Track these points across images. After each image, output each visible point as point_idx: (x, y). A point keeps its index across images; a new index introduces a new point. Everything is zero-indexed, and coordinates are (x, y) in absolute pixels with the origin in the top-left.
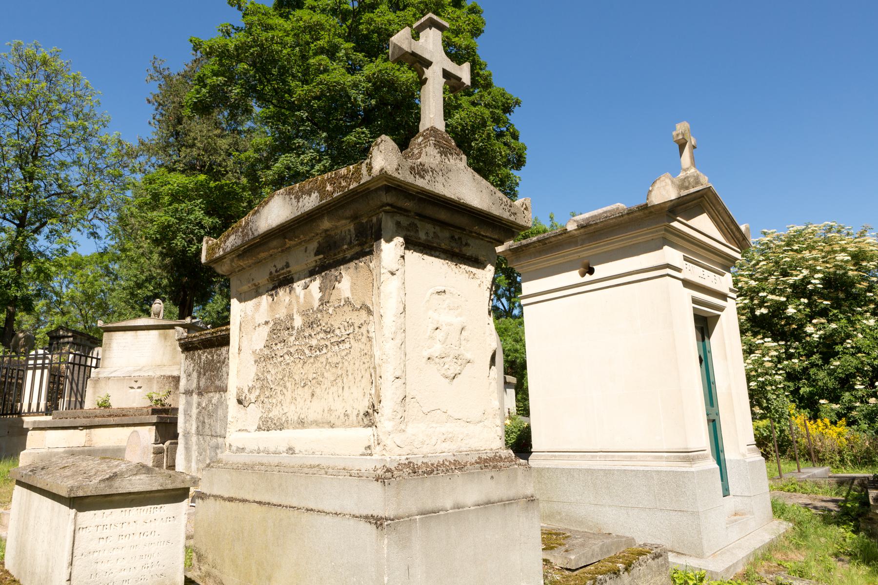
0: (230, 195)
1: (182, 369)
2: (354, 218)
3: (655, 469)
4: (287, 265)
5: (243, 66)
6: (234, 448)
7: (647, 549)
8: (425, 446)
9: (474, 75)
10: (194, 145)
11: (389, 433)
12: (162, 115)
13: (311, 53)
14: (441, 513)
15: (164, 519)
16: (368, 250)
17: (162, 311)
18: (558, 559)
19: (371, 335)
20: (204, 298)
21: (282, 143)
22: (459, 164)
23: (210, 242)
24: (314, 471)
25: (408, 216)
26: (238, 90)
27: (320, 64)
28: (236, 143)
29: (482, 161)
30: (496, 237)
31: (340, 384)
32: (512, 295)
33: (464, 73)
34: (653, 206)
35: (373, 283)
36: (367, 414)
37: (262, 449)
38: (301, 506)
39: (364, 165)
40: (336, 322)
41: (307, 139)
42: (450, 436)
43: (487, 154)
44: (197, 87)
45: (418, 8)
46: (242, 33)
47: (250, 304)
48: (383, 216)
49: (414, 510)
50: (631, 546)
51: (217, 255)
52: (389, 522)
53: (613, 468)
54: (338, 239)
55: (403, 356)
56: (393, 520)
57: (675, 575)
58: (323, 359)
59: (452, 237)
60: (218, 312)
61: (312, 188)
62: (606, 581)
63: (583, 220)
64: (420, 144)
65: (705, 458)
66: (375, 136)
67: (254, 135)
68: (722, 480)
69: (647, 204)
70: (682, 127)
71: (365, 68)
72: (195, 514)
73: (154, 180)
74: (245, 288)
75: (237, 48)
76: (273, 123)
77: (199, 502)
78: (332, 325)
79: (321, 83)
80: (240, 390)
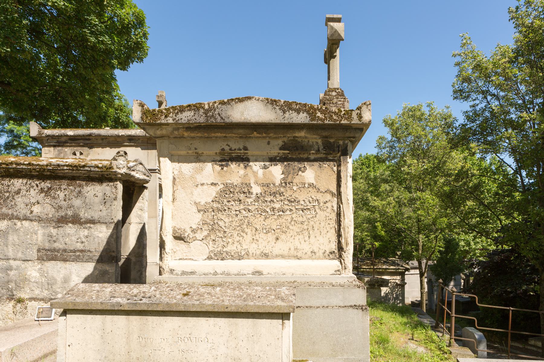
49: (335, 304)
68: (140, 311)
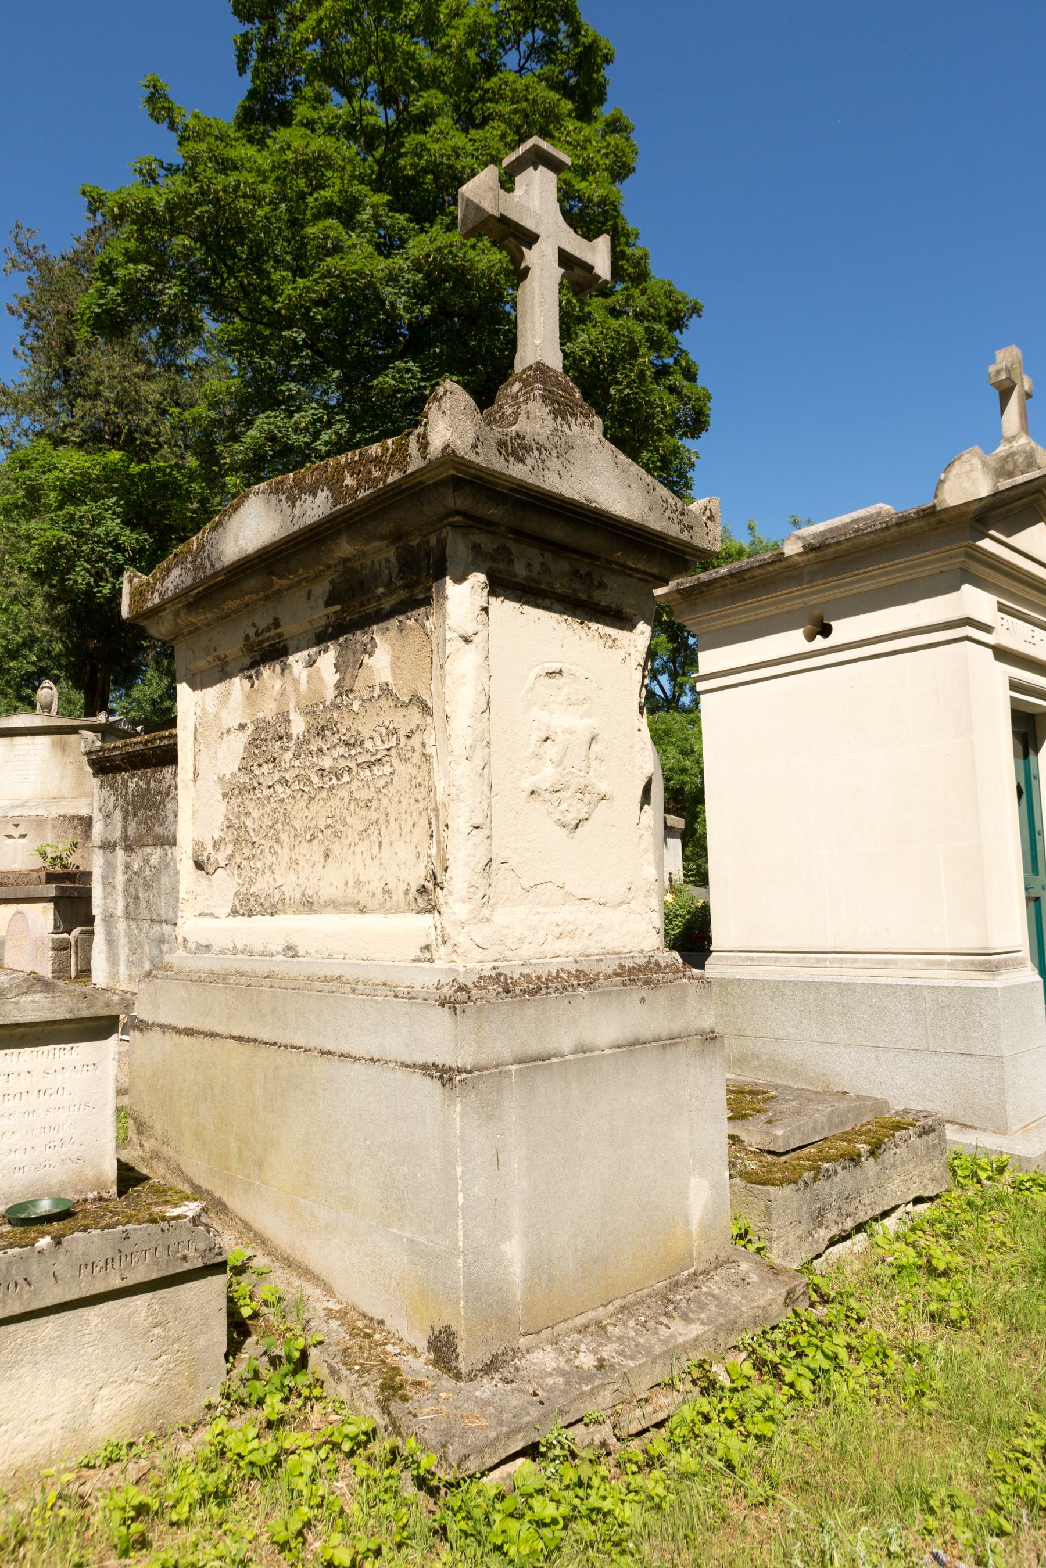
0: (166, 489)
1: (96, 805)
2: (397, 537)
3: (929, 982)
4: (276, 624)
5: (182, 241)
6: (191, 945)
7: (909, 1118)
8: (525, 945)
9: (617, 256)
10: (96, 395)
11: (463, 924)
12: (37, 337)
13: (309, 215)
14: (554, 1060)
15: (79, 1068)
16: (421, 596)
17: (55, 702)
18: (753, 1136)
19: (429, 750)
20: (129, 676)
21: (258, 390)
22: (588, 433)
23: (136, 580)
24: (333, 987)
25: (494, 533)
26: (174, 290)
27: (327, 237)
28: (175, 391)
29: (630, 425)
30: (655, 571)
31: (375, 837)
32: (680, 671)
33: (598, 255)
34: (946, 510)
35: (432, 658)
36: (423, 890)
37: (240, 947)
38: (312, 1045)
39: (413, 439)
40: (366, 727)
41: (304, 382)
42: (570, 927)
43: (637, 409)
44: (99, 284)
45: (509, 123)
46: (179, 178)
47: (212, 693)
48: (447, 533)
49: (507, 1055)
50: (882, 1113)
51: (150, 605)
52: (464, 1075)
53: (855, 980)
54: (367, 576)
55: (486, 789)
56: (470, 1072)
57: (956, 1162)
58: (344, 793)
59: (576, 572)
60: (154, 702)
61: (317, 481)
62: (836, 1173)
63: (815, 536)
64: (515, 397)
65: (1018, 964)
66: (433, 374)
67: (207, 374)
69: (934, 507)
70: (1007, 357)
71: (411, 243)
72: (129, 1053)
73: (28, 462)
74: (202, 664)
75: (170, 206)
76: (241, 352)
77: (135, 1035)
78: (358, 733)
79: (329, 274)
80: (199, 846)
